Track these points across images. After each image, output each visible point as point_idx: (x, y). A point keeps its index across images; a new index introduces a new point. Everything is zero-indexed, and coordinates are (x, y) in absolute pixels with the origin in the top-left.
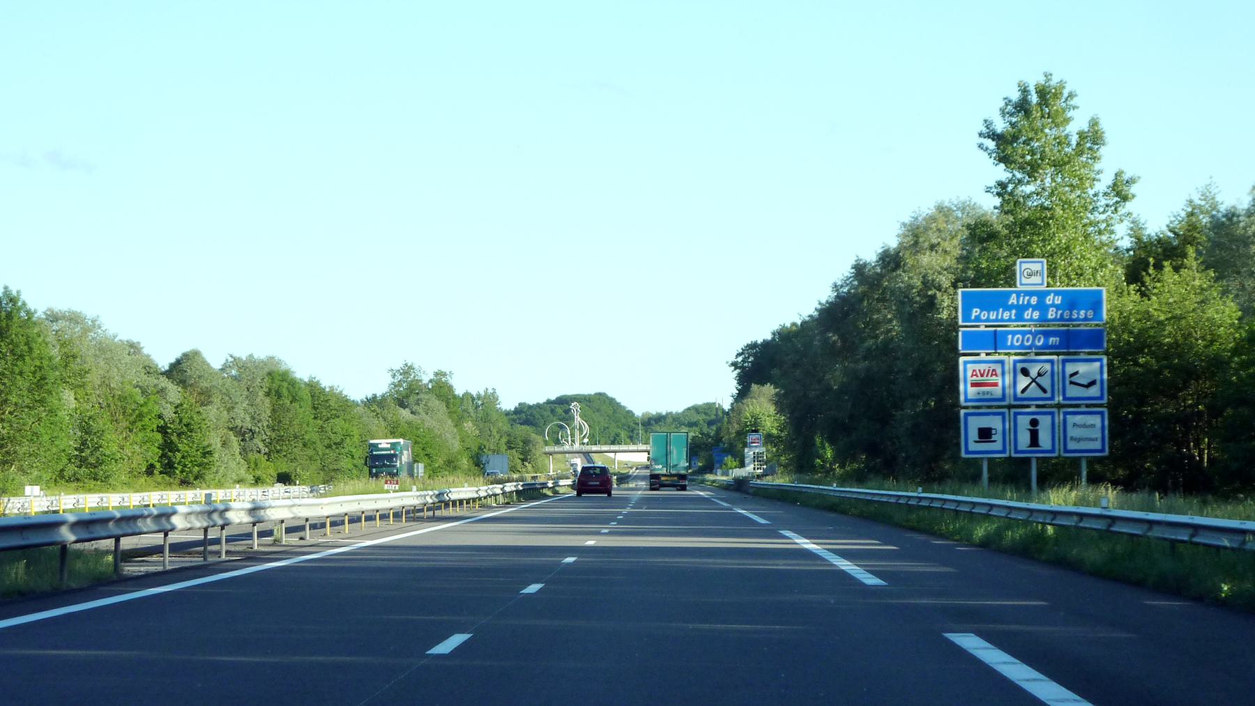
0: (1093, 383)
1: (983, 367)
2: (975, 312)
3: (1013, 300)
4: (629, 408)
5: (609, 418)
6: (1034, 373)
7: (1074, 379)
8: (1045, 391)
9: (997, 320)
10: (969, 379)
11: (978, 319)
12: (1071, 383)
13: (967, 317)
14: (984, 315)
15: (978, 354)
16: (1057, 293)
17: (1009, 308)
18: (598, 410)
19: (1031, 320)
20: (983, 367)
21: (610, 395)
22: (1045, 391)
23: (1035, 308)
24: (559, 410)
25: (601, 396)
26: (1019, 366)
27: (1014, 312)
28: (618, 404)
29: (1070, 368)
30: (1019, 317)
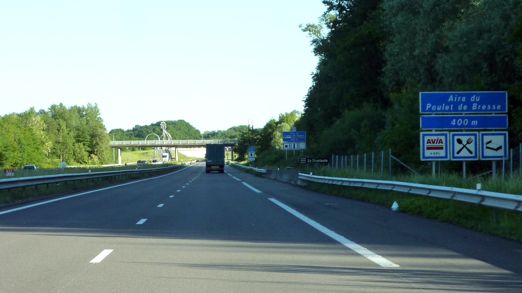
0: (500, 148)
1: (434, 138)
2: (429, 106)
3: (451, 99)
4: (197, 128)
5: (182, 130)
6: (464, 142)
7: (489, 145)
8: (471, 153)
9: (441, 111)
10: (426, 145)
11: (430, 110)
12: (487, 148)
13: (424, 107)
14: (434, 108)
15: (431, 131)
16: (477, 95)
17: (450, 104)
18: (180, 129)
19: (463, 110)
20: (434, 138)
21: (187, 121)
22: (471, 153)
23: (464, 104)
24: (157, 129)
25: (182, 122)
26: (456, 138)
27: (452, 106)
28: (191, 127)
29: (487, 139)
30: (455, 109)
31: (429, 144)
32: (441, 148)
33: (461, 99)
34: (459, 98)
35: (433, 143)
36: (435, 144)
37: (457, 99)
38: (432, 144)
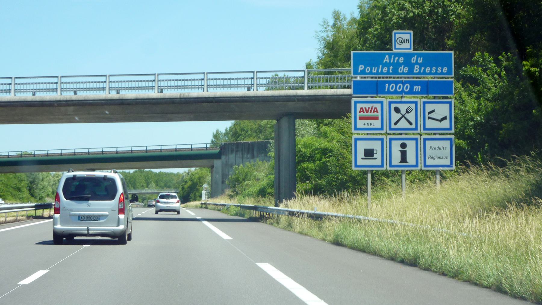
31: (362, 113)
32: (376, 118)
33: (398, 60)
34: (396, 58)
36: (369, 113)
37: (394, 60)
38: (365, 113)
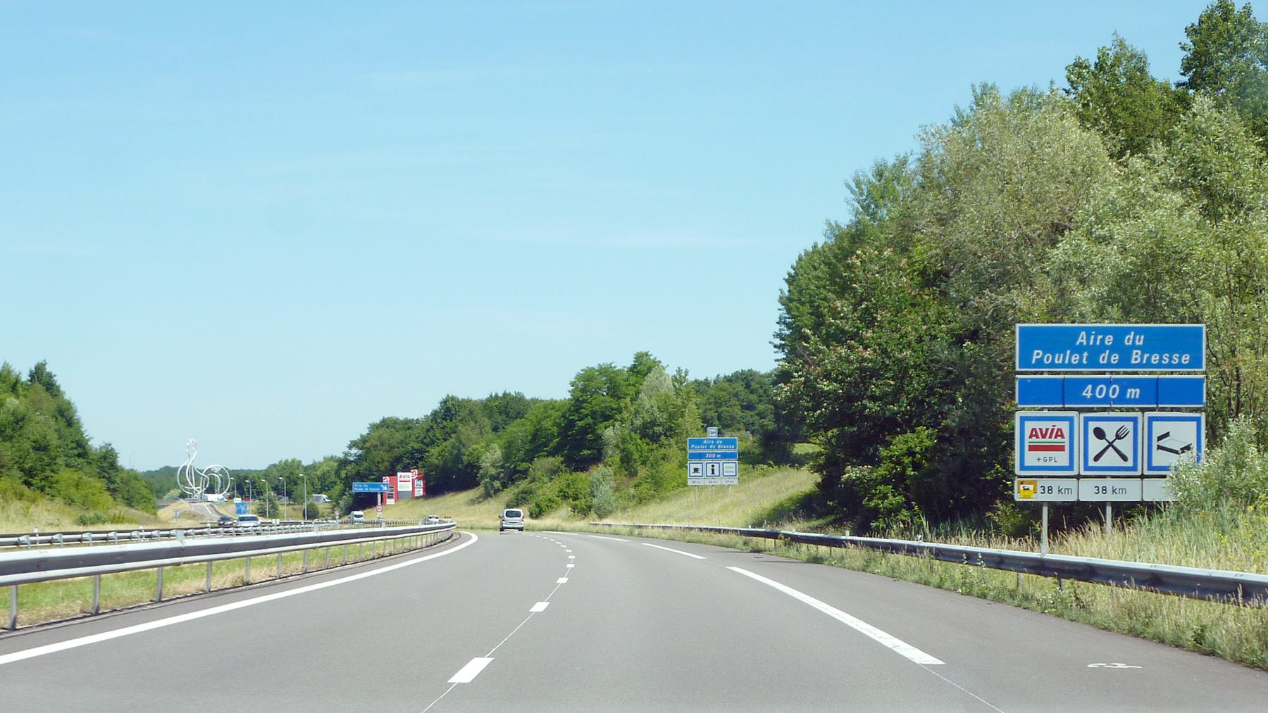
31: (1034, 439)
32: (1061, 448)
33: (1103, 340)
34: (1100, 337)
35: (1044, 436)
36: (1047, 439)
37: (1095, 340)
38: (1041, 439)
